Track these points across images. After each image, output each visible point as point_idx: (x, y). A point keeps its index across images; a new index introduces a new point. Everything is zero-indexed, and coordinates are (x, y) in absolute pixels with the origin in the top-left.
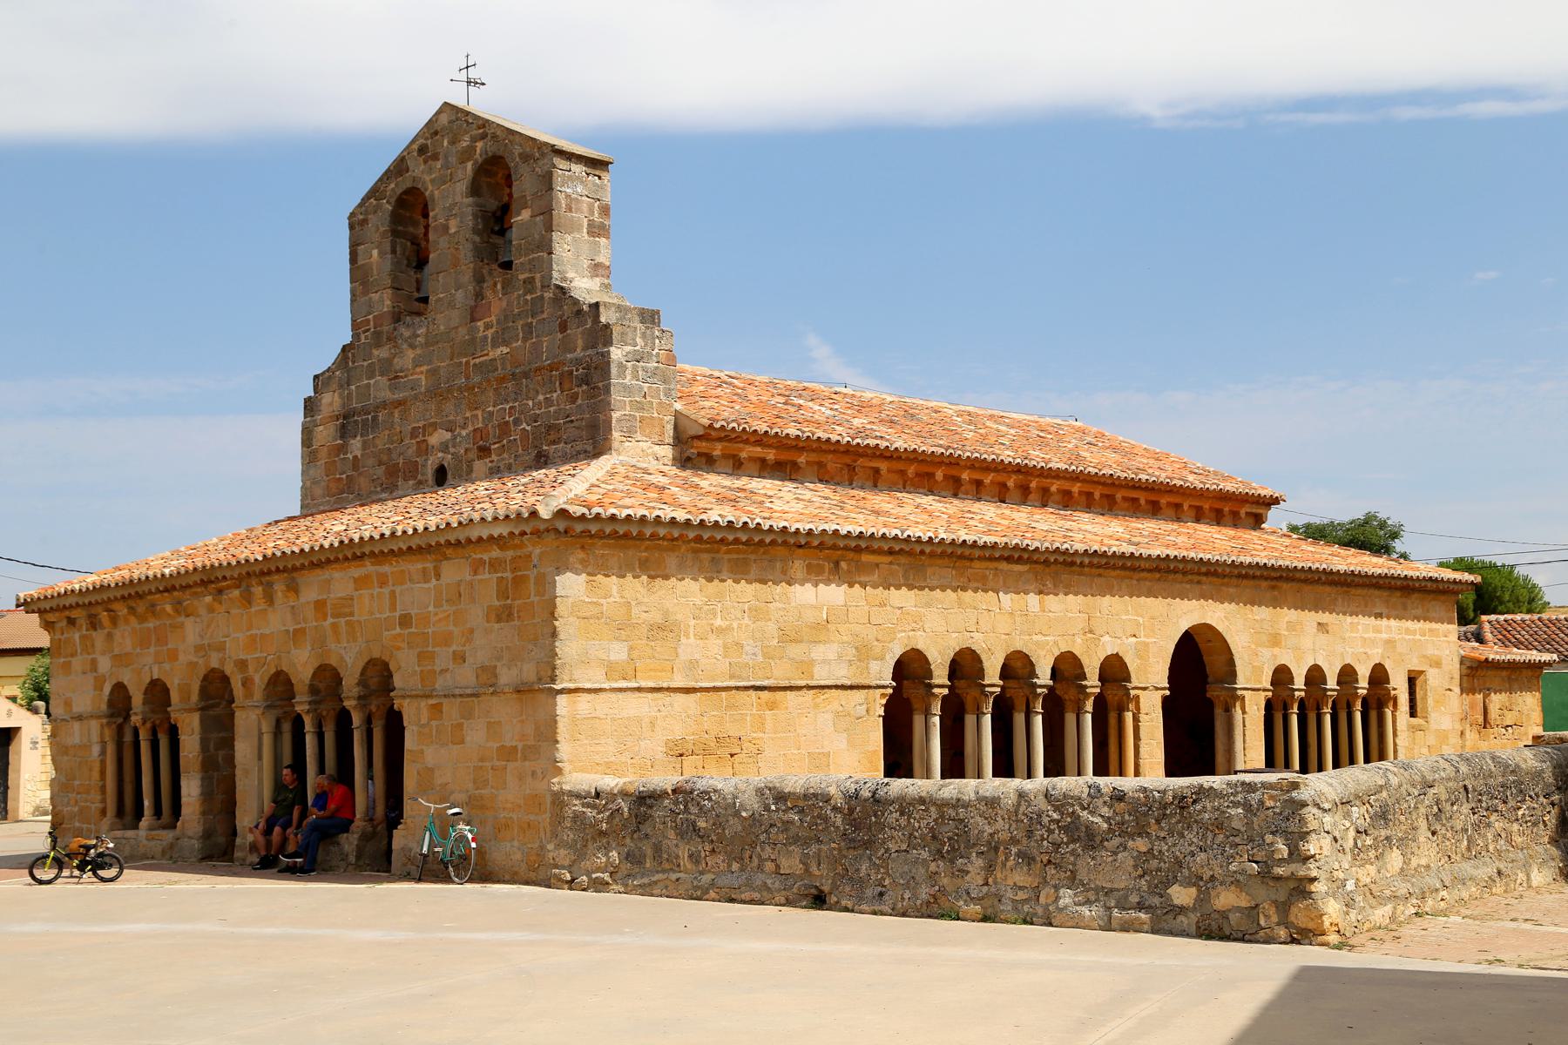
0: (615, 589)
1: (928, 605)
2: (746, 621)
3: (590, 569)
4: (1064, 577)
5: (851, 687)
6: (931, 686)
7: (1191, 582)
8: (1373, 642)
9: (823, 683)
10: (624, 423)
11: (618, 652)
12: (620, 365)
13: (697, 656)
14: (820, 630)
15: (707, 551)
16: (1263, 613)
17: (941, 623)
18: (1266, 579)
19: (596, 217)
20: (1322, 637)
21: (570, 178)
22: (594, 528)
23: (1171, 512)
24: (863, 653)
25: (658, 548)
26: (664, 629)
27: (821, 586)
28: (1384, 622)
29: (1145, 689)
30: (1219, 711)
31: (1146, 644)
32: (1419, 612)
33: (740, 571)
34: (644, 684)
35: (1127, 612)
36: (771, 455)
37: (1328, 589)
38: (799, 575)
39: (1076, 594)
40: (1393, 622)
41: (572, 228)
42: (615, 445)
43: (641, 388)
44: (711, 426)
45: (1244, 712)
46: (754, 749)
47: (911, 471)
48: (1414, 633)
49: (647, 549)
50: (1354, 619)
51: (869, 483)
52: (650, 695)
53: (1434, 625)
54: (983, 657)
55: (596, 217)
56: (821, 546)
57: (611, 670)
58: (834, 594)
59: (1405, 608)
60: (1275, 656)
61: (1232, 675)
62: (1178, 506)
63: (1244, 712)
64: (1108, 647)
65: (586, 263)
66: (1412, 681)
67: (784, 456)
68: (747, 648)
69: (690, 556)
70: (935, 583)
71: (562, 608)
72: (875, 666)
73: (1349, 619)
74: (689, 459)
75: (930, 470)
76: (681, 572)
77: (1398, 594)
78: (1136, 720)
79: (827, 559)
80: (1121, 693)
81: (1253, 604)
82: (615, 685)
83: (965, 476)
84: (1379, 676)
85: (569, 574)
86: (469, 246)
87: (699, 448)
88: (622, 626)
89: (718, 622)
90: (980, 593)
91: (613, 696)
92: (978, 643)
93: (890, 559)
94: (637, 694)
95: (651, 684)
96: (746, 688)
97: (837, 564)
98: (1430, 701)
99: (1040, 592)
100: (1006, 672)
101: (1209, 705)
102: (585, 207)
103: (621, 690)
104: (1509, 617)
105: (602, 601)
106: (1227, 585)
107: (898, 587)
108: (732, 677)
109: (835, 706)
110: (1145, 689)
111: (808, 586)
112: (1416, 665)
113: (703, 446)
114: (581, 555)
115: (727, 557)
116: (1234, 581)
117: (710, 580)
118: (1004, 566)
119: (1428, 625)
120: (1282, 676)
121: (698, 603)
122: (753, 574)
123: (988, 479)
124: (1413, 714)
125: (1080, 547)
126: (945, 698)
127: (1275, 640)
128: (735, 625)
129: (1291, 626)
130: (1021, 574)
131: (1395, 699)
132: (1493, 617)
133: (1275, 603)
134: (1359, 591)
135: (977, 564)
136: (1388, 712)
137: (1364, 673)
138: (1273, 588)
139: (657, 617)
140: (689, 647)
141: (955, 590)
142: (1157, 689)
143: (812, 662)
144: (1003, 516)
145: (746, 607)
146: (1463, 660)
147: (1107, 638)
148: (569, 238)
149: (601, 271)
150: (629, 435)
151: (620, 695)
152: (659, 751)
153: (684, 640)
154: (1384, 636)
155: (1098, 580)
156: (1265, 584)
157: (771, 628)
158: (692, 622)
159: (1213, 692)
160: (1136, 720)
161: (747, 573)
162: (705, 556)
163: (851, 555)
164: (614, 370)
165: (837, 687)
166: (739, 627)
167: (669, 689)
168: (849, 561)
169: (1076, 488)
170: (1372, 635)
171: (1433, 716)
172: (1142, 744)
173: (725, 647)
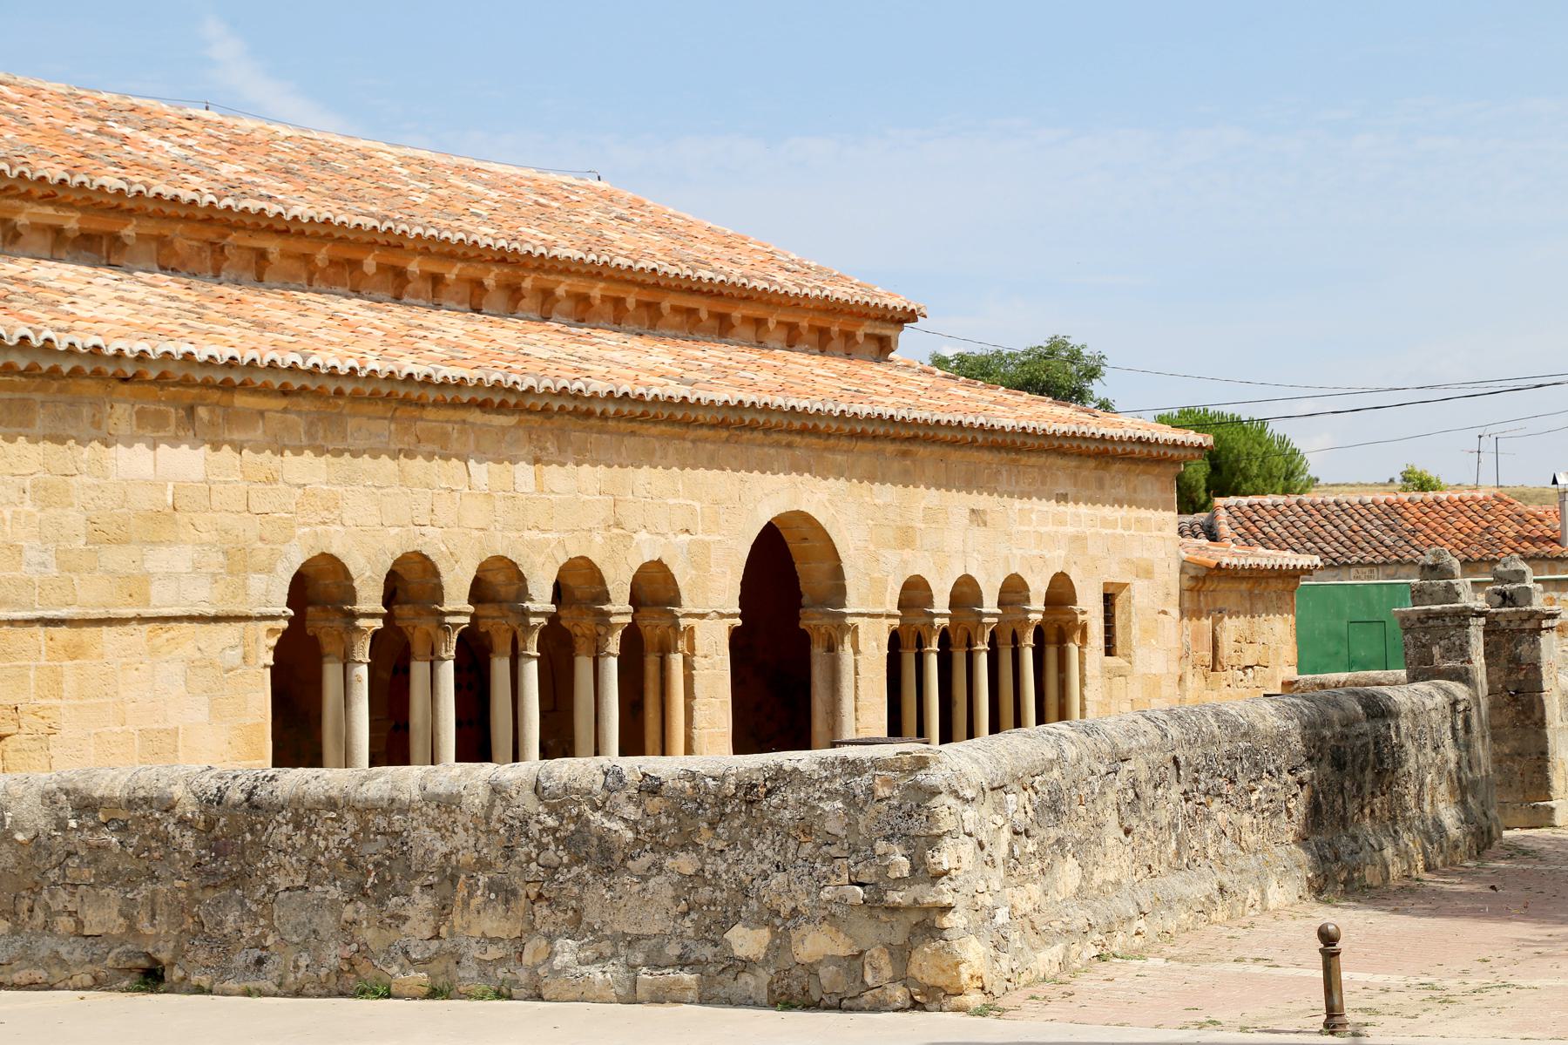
1: (349, 481)
2: (28, 507)
5: (217, 619)
7: (777, 444)
9: (166, 612)
14: (161, 523)
16: (887, 494)
17: (375, 512)
18: (894, 440)
20: (978, 532)
23: (748, 332)
24: (237, 560)
27: (163, 448)
29: (702, 616)
30: (818, 651)
31: (706, 545)
32: (1121, 492)
35: (676, 493)
36: (72, 222)
37: (987, 456)
39: (594, 463)
45: (856, 651)
47: (322, 256)
48: (1114, 524)
50: (1026, 504)
51: (250, 275)
53: (1143, 513)
58: (186, 462)
60: (905, 563)
63: (856, 651)
64: (646, 550)
66: (1109, 600)
67: (97, 224)
68: (29, 554)
70: (361, 444)
72: (257, 583)
73: (1017, 504)
77: (1092, 463)
78: (688, 666)
79: (173, 401)
80: (665, 623)
81: (872, 480)
83: (414, 267)
84: (1061, 593)
92: (433, 544)
93: (281, 403)
96: (29, 622)
97: (191, 410)
99: (537, 461)
104: (1254, 499)
106: (832, 450)
107: (298, 451)
109: (188, 650)
110: (702, 616)
111: (140, 447)
116: (844, 443)
118: (476, 416)
120: (914, 594)
123: (452, 273)
124: (1109, 651)
127: (906, 538)
129: (930, 515)
130: (504, 430)
131: (1084, 628)
132: (1232, 500)
134: (1033, 460)
135: (430, 413)
136: (1073, 648)
137: (1038, 588)
138: (905, 454)
141: (394, 456)
142: (722, 616)
143: (147, 578)
144: (1105, 522)
145: (28, 483)
147: (643, 535)
154: (1070, 530)
155: (630, 442)
156: (890, 448)
157: (74, 519)
159: (810, 620)
160: (688, 666)
161: (29, 424)
165: (191, 618)
168: (212, 407)
169: (597, 291)
170: (1050, 528)
171: (1139, 654)
172: (698, 705)
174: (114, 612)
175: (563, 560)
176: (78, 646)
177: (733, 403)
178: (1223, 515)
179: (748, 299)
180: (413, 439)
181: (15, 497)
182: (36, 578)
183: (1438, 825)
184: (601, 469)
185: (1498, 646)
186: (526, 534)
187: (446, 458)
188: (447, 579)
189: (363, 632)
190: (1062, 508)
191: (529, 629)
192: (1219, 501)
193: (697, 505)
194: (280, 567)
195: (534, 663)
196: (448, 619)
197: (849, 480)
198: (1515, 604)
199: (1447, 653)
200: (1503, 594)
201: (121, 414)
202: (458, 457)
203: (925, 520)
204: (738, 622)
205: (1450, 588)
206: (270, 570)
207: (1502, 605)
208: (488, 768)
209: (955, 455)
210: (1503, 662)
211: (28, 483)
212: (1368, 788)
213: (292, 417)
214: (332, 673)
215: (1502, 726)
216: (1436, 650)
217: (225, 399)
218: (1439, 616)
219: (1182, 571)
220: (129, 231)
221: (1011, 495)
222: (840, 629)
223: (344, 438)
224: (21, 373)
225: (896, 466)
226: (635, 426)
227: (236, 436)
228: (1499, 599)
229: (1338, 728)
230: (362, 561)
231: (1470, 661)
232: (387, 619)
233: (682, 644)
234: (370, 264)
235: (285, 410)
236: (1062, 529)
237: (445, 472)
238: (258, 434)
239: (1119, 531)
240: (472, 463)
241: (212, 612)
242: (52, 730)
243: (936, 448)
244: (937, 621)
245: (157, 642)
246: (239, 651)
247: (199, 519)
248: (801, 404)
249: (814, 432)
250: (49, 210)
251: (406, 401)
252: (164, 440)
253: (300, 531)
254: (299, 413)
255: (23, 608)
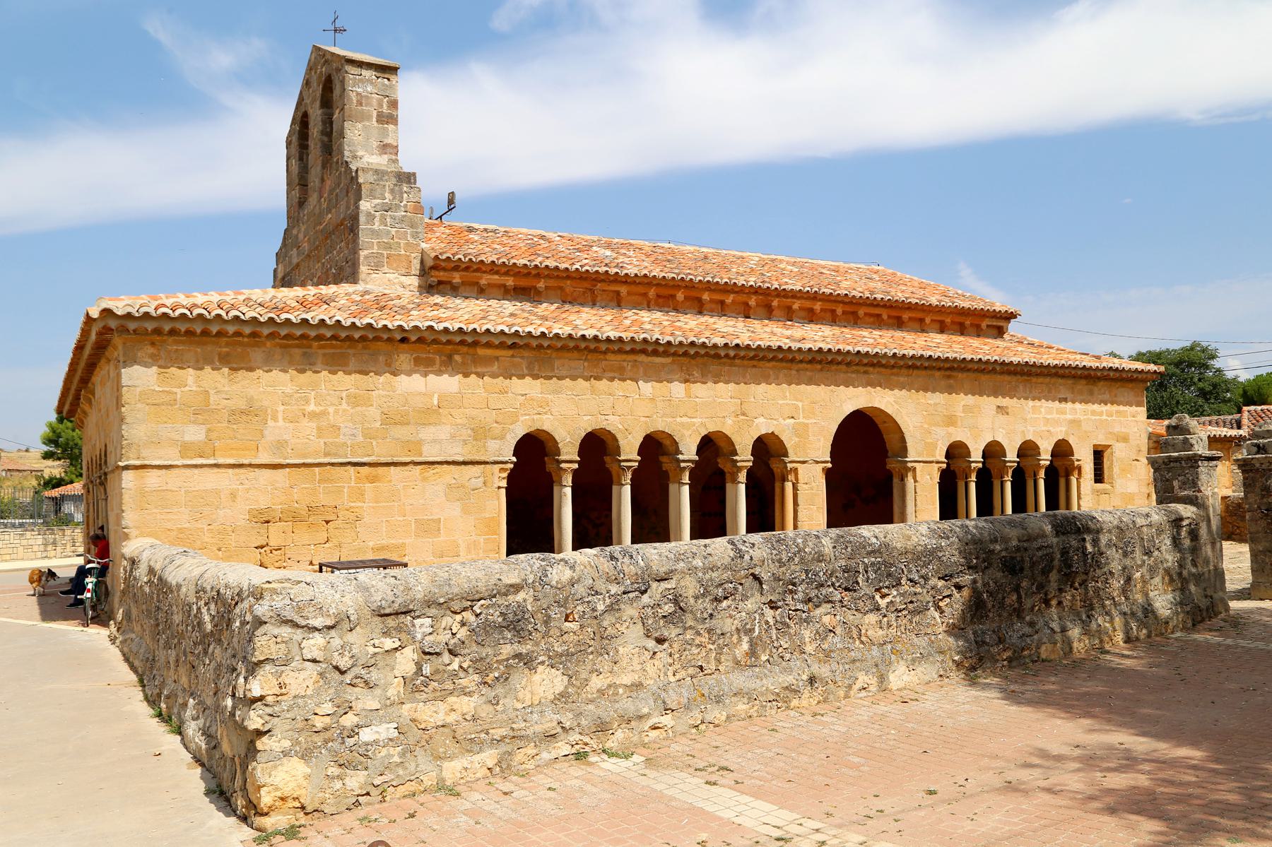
0: (190, 380)
1: (556, 392)
2: (344, 406)
3: (161, 362)
4: (712, 368)
5: (465, 463)
6: (679, 461)
7: (857, 372)
8: (1057, 422)
9: (431, 459)
10: (371, 260)
11: (194, 434)
12: (369, 214)
13: (286, 437)
14: (429, 415)
15: (298, 346)
16: (936, 399)
17: (567, 410)
18: (940, 369)
19: (385, 109)
20: (1002, 418)
21: (361, 81)
22: (183, 327)
23: (917, 325)
24: (480, 433)
25: (241, 344)
26: (250, 413)
27: (431, 376)
28: (1069, 405)
29: (804, 462)
30: (896, 481)
31: (806, 425)
32: (1107, 396)
33: (336, 364)
34: (221, 461)
35: (785, 398)
36: (510, 282)
37: (1007, 378)
38: (405, 366)
39: (727, 382)
40: (1077, 405)
41: (363, 117)
42: (362, 276)
43: (389, 232)
44: (437, 257)
45: (916, 481)
46: (352, 516)
47: (652, 293)
48: (1101, 414)
49: (227, 344)
50: (1037, 403)
51: (614, 304)
52: (230, 471)
53: (1121, 408)
54: (619, 436)
55: (385, 109)
56: (421, 340)
57: (185, 449)
58: (446, 384)
59: (1091, 393)
60: (950, 434)
61: (904, 450)
62: (922, 320)
63: (916, 481)
64: (762, 427)
65: (375, 144)
66: (1098, 455)
67: (523, 283)
68: (343, 430)
69: (278, 350)
70: (564, 373)
71: (126, 395)
72: (493, 445)
73: (1031, 403)
74: (431, 286)
75: (671, 292)
76: (268, 364)
77: (1083, 382)
78: (795, 488)
79: (439, 352)
80: (781, 466)
81: (926, 390)
82: (189, 462)
83: (706, 296)
84: (1062, 450)
85: (136, 367)
86: (319, 145)
87: (440, 277)
88: (201, 410)
89: (312, 407)
90: (616, 382)
91: (188, 472)
92: (613, 423)
93: (510, 352)
94: (216, 470)
95: (232, 461)
96: (342, 464)
97: (450, 357)
98: (1116, 470)
99: (686, 381)
100: (986, 454)
101: (889, 476)
102: (375, 102)
103: (196, 466)
104: (1264, 407)
105: (178, 390)
106: (897, 375)
107: (521, 377)
108: (326, 455)
109: (448, 479)
110: (804, 462)
111: (416, 376)
112: (1101, 440)
113: (442, 275)
114: (151, 350)
115: (321, 351)
116: (904, 371)
117: (302, 371)
118: (642, 358)
119: (1115, 408)
120: (956, 452)
121: (288, 390)
122: (353, 363)
123: (730, 299)
124: (1099, 477)
125: (720, 341)
126: (575, 472)
127: (951, 421)
128: (331, 410)
129: (967, 409)
130: (663, 365)
131: (1079, 468)
132: (1252, 408)
133: (950, 390)
134: (1041, 380)
135: (610, 356)
136: (1074, 480)
138: (949, 377)
139: (242, 404)
140: (277, 429)
141: (587, 379)
142: (817, 462)
143: (420, 443)
144: (1094, 413)
145: (344, 394)
146: (1150, 436)
147: (761, 420)
148: (359, 125)
149: (388, 150)
150: (377, 268)
151: (196, 471)
152: (242, 519)
153: (271, 423)
154: (1069, 417)
156: (938, 374)
157: (373, 412)
158: (281, 408)
159: (892, 465)
160: (795, 488)
161: (346, 365)
162: (297, 352)
163: (465, 349)
164: (362, 219)
165: (448, 463)
166: (336, 412)
167: (250, 465)
168: (463, 355)
169: (818, 306)
170: (1055, 416)
171: (1119, 483)
172: (800, 509)
173: (319, 429)
174: (396, 459)
175: (704, 433)
176: (376, 477)
177: (785, 347)
178: (1246, 415)
179: (909, 308)
180: (600, 370)
181: (336, 402)
182: (349, 443)
183: (1148, 610)
184: (732, 386)
185: (1254, 480)
186: (679, 419)
187: (624, 380)
188: (622, 442)
189: (565, 470)
190: (1063, 405)
191: (740, 469)
192: (1245, 408)
193: (800, 404)
194: (508, 437)
195: (687, 487)
196: (563, 465)
197: (909, 390)
198: (1266, 452)
199: (1183, 486)
200: (1257, 446)
201: (404, 359)
202: (632, 380)
203: (964, 411)
204: (830, 465)
205: (1186, 441)
206: (502, 438)
207: (1258, 453)
208: (958, 522)
209: (984, 378)
210: (1258, 490)
211: (344, 394)
212: (1053, 585)
213: (517, 360)
214: (672, 488)
215: (1258, 532)
216: (1176, 483)
217: (471, 351)
218: (1177, 460)
219: (1149, 438)
220: (541, 285)
221: (1026, 399)
222: (905, 470)
223: (553, 370)
224: (328, 339)
225: (943, 383)
226: (755, 363)
227: (479, 370)
228: (1255, 449)
229: (1015, 543)
230: (564, 434)
231: (1200, 491)
232: (983, 463)
233: (792, 477)
234: (680, 296)
235: (513, 356)
236: (1062, 416)
237: (620, 388)
238: (495, 368)
239: (1104, 417)
240: (641, 383)
241: (461, 459)
242: (358, 519)
243: (970, 374)
244: (973, 465)
245: (426, 474)
246: (481, 479)
247: (453, 412)
248: (863, 349)
249: (879, 365)
250: (496, 277)
251: (596, 350)
252: (432, 372)
253: (522, 418)
254: (522, 357)
255: (340, 457)
